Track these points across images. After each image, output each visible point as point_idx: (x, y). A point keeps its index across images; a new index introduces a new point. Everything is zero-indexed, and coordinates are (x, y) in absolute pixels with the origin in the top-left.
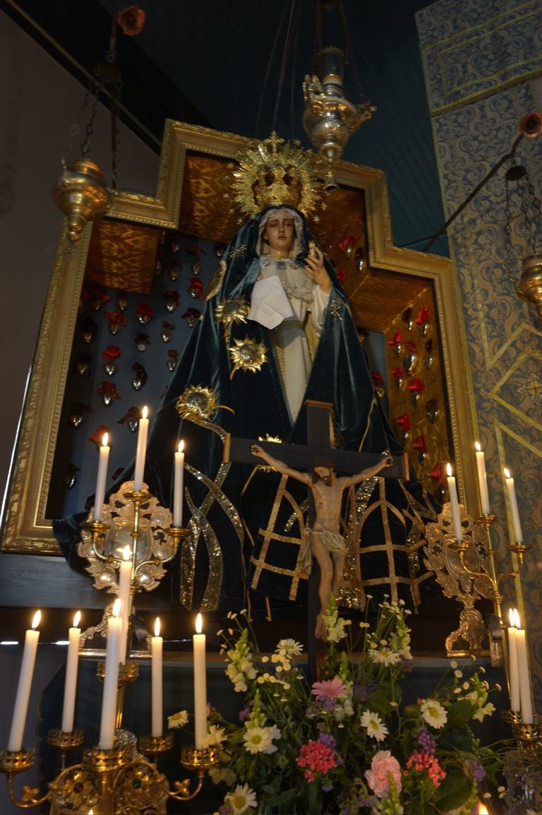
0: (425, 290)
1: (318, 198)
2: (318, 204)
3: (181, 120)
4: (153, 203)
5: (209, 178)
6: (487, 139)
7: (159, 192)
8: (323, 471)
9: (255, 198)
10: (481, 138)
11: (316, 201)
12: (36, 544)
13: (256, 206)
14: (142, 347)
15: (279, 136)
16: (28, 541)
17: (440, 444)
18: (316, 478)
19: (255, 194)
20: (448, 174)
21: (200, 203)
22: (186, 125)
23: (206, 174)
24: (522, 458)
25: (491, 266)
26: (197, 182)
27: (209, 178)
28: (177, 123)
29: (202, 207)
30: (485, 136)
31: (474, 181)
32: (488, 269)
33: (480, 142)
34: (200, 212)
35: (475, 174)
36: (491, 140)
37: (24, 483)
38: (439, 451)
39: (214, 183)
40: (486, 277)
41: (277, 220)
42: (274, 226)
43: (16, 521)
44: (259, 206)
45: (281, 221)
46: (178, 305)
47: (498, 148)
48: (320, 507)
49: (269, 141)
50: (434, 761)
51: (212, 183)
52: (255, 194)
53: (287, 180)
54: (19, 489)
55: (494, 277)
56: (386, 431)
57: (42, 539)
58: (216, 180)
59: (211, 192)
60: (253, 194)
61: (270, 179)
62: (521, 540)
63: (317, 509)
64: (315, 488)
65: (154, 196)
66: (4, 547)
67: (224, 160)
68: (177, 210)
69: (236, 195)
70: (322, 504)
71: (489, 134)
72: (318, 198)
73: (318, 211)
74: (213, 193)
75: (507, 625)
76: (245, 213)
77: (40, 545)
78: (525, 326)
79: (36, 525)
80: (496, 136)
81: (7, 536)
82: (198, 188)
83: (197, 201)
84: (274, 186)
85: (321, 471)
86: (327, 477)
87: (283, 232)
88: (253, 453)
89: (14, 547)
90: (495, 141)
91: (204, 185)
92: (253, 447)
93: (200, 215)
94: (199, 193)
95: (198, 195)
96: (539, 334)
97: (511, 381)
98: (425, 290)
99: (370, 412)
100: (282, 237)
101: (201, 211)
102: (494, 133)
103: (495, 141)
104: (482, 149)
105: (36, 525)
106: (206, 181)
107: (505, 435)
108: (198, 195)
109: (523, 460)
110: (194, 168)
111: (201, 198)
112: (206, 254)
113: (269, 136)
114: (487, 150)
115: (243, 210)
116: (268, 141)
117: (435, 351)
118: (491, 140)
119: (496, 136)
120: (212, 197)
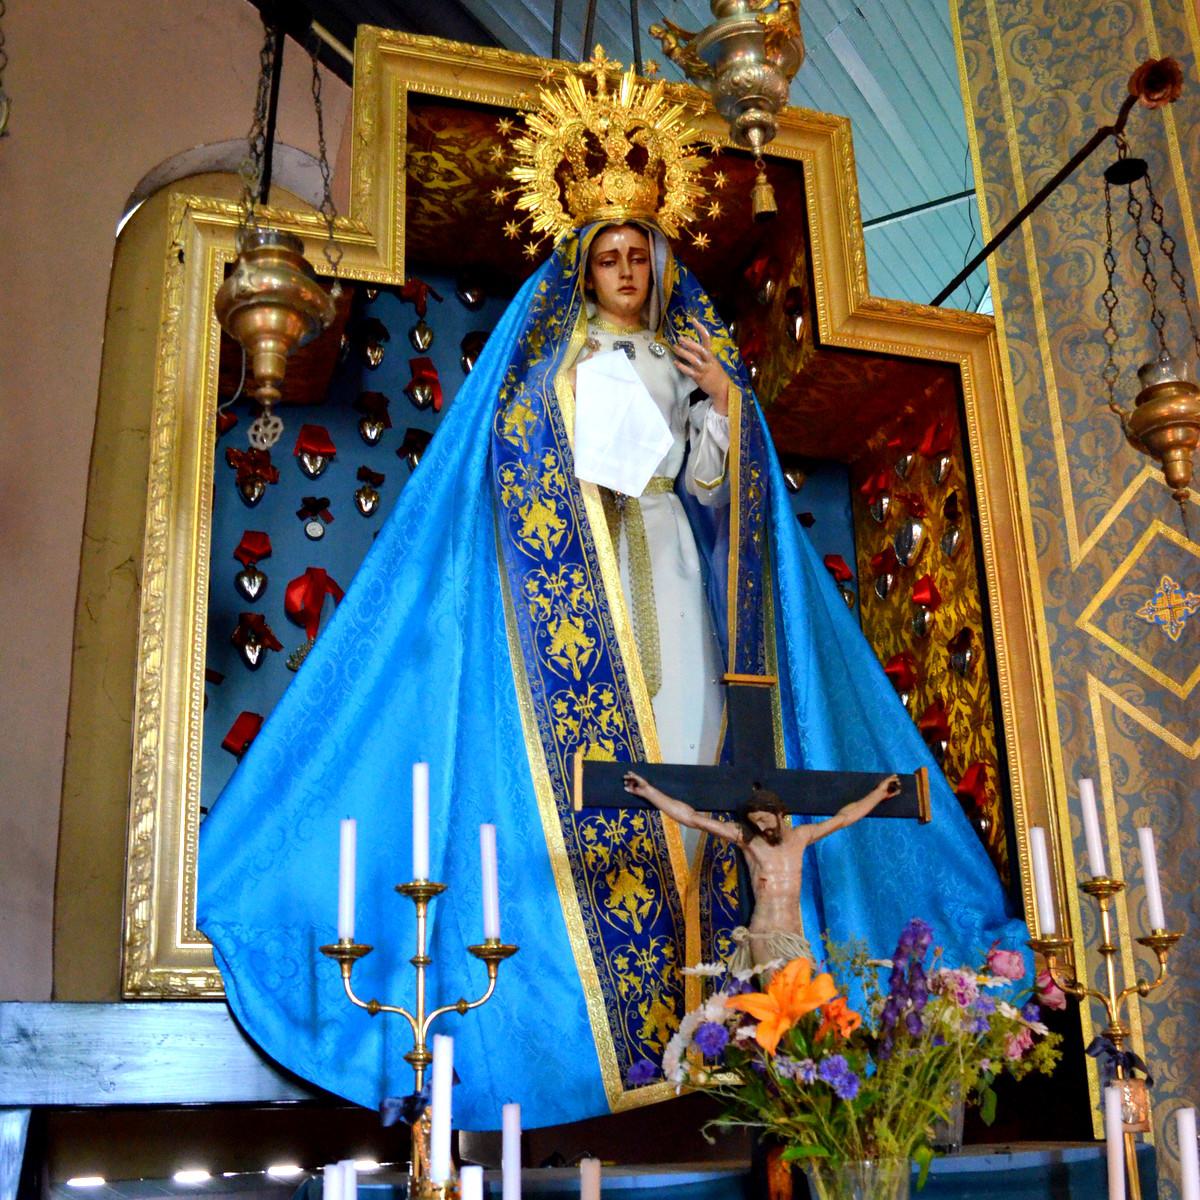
0: (940, 380)
1: (702, 192)
2: (700, 206)
5: (456, 150)
6: (1072, 36)
8: (764, 819)
9: (562, 199)
10: (1058, 33)
11: (698, 199)
12: (191, 981)
13: (566, 217)
14: (315, 529)
16: (176, 975)
17: (976, 722)
18: (752, 831)
19: (563, 190)
20: (986, 120)
23: (448, 142)
24: (1038, 75)
25: (1030, 37)
26: (425, 158)
27: (456, 150)
29: (451, 166)
30: (1067, 28)
31: (1044, 135)
32: (1024, 43)
33: (1057, 44)
34: (446, 180)
35: (1046, 120)
36: (1080, 40)
37: (153, 860)
38: (974, 738)
39: (465, 159)
40: (1020, 59)
42: (608, 264)
43: (146, 940)
44: (573, 216)
46: (387, 425)
47: (1096, 60)
48: (760, 887)
51: (461, 161)
53: (637, 159)
54: (146, 875)
55: (1035, 58)
57: (199, 970)
58: (471, 154)
59: (457, 178)
61: (596, 161)
63: (755, 890)
64: (750, 850)
66: (130, 991)
67: (493, 113)
69: (520, 194)
70: (764, 880)
71: (1076, 25)
72: (702, 192)
73: (703, 224)
74: (463, 180)
76: (543, 232)
77: (199, 982)
78: (1158, 527)
79: (184, 940)
80: (1091, 32)
81: (133, 970)
82: (428, 169)
83: (427, 197)
84: (609, 177)
85: (760, 819)
86: (772, 830)
87: (630, 278)
88: (627, 789)
89: (151, 989)
90: (1090, 42)
91: (443, 164)
92: (626, 777)
94: (431, 180)
96: (1190, 546)
97: (1069, 246)
98: (940, 380)
100: (629, 290)
101: (449, 175)
102: (1088, 22)
103: (1090, 42)
104: (1086, 207)
105: (184, 940)
106: (447, 156)
107: (1082, 540)
109: (1040, 80)
111: (437, 191)
112: (440, 299)
114: (1071, 63)
115: (537, 227)
117: (964, 524)
118: (1080, 40)
119: (1091, 32)
120: (460, 188)
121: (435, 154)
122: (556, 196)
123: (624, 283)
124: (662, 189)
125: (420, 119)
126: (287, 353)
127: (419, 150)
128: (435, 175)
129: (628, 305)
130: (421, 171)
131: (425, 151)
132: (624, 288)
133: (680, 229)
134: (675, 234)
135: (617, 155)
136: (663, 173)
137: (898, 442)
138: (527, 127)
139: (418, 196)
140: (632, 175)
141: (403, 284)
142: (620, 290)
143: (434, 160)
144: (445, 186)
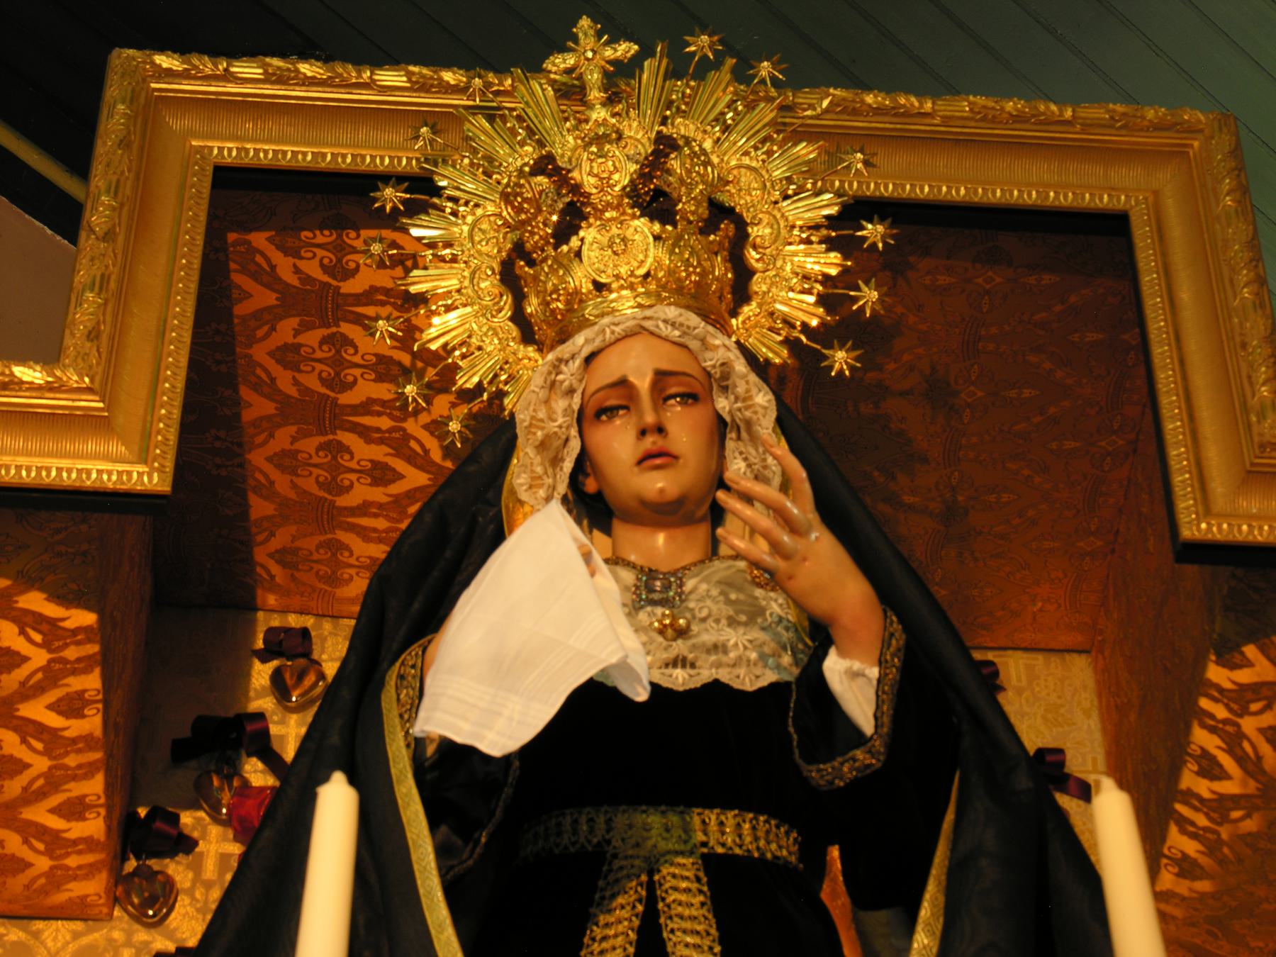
3: (181, 48)
4: (49, 388)
7: (74, 340)
9: (519, 317)
13: (531, 351)
15: (613, 31)
19: (519, 300)
21: (366, 434)
22: (206, 65)
28: (164, 61)
29: (379, 452)
34: (376, 482)
41: (623, 383)
45: (643, 384)
49: (571, 61)
50: (698, 222)
52: (519, 300)
56: (169, 70)
60: (507, 300)
62: (337, 504)
65: (49, 356)
68: (169, 412)
75: (542, 464)
82: (339, 363)
87: (660, 430)
91: (365, 452)
93: (378, 495)
94: (352, 273)
95: (346, 398)
99: (795, 743)
101: (380, 474)
108: (346, 398)
110: (307, 279)
111: (364, 509)
113: (563, 41)
116: (559, 63)
121: (347, 329)
122: (507, 312)
123: (650, 442)
124: (743, 274)
125: (301, 378)
126: (230, 834)
127: (308, 435)
128: (353, 477)
129: (662, 491)
130: (328, 371)
131: (323, 432)
132: (648, 456)
133: (791, 343)
134: (777, 356)
135: (605, 183)
136: (741, 238)
137: (849, 263)
138: (438, 191)
139: (333, 531)
140: (641, 223)
141: (166, 488)
142: (640, 462)
143: (343, 448)
144: (378, 495)
